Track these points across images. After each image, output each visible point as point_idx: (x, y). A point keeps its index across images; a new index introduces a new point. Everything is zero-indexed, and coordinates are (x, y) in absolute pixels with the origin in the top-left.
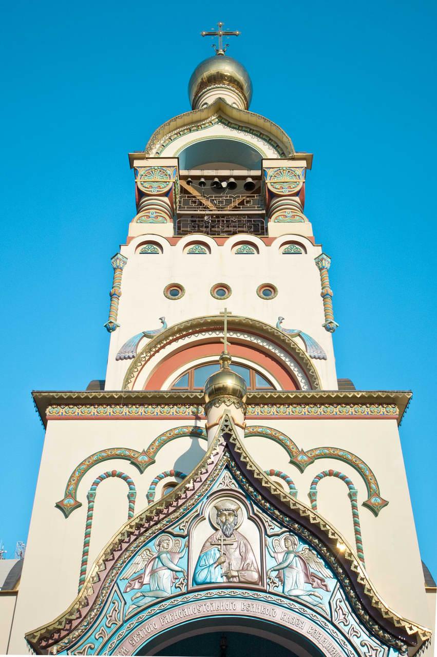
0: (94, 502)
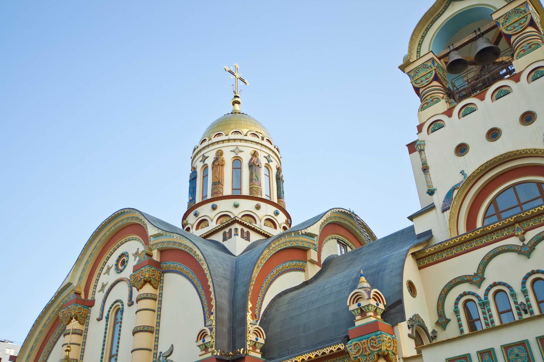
0: (459, 315)
